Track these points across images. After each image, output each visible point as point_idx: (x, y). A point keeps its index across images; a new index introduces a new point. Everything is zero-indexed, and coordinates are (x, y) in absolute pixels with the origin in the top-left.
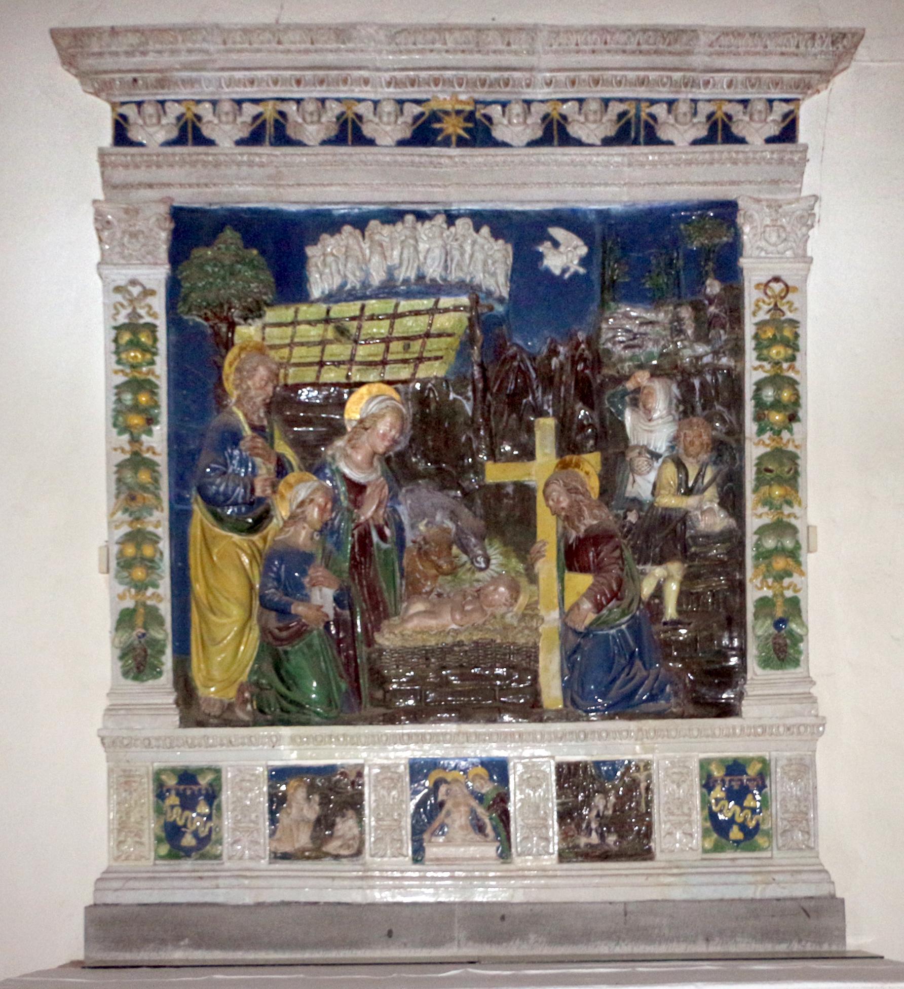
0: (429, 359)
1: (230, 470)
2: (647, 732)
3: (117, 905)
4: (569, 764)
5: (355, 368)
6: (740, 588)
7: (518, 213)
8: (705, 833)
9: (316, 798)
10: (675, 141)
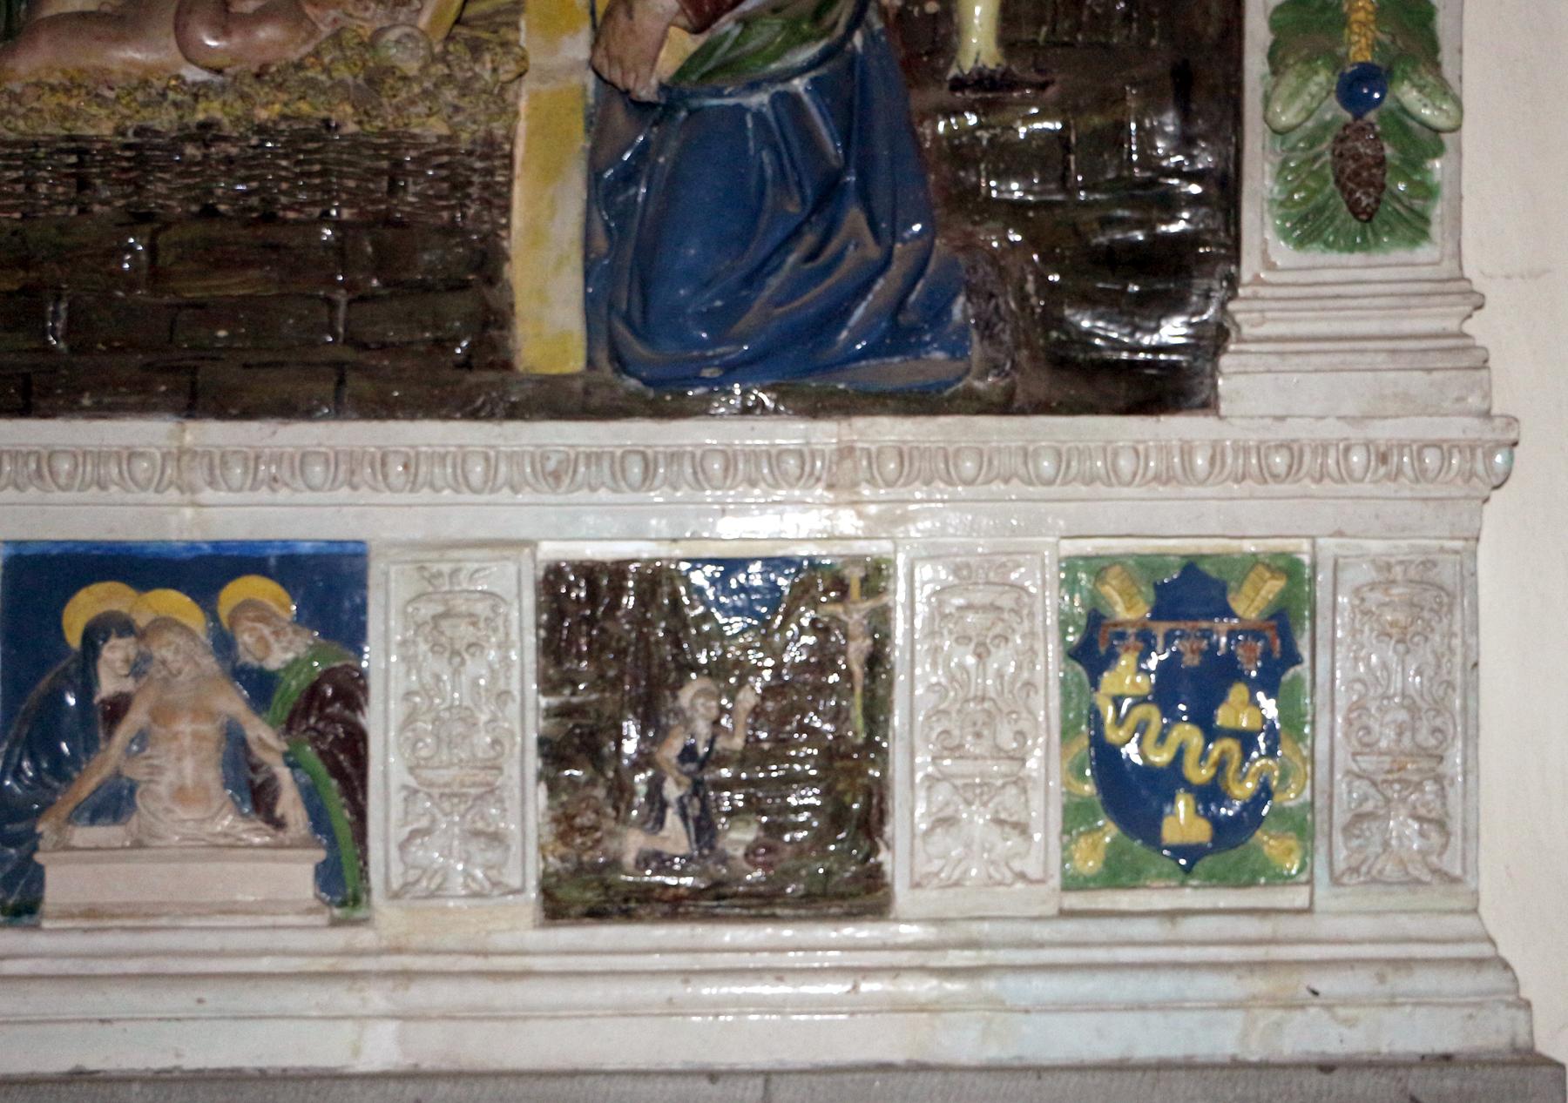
4: (589, 571)
8: (1075, 816)
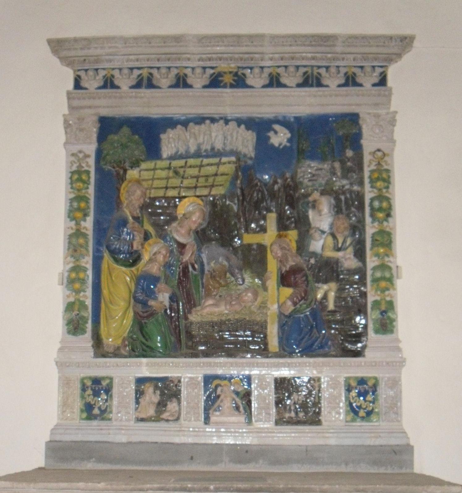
0: (217, 186)
1: (122, 238)
5: (182, 190)
8: (347, 413)
9: (158, 392)
10: (330, 85)
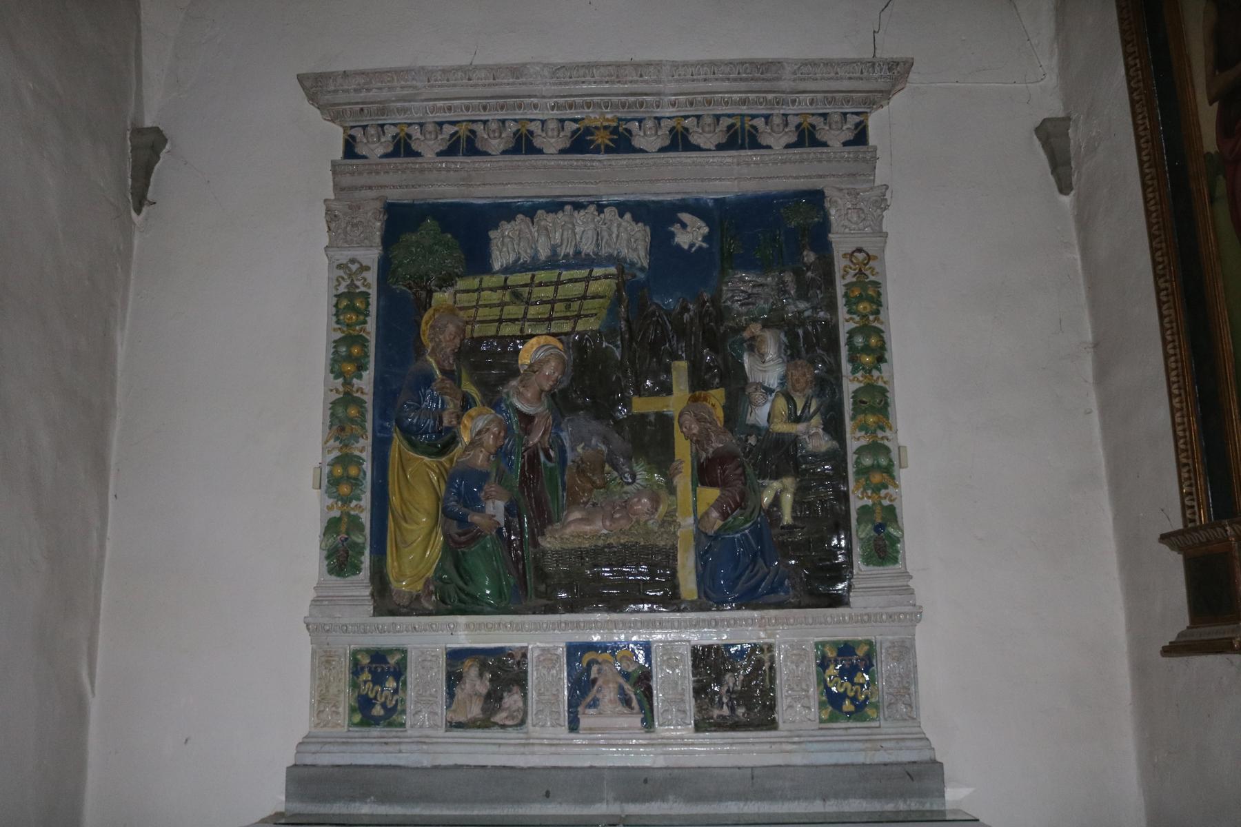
0: (586, 316)
2: (769, 620)
3: (314, 766)
6: (844, 498)
7: (653, 202)
8: (822, 705)
